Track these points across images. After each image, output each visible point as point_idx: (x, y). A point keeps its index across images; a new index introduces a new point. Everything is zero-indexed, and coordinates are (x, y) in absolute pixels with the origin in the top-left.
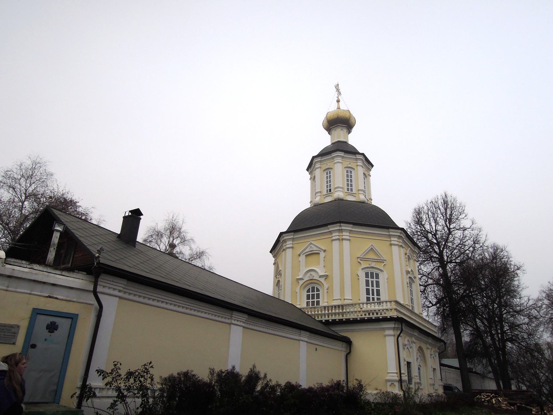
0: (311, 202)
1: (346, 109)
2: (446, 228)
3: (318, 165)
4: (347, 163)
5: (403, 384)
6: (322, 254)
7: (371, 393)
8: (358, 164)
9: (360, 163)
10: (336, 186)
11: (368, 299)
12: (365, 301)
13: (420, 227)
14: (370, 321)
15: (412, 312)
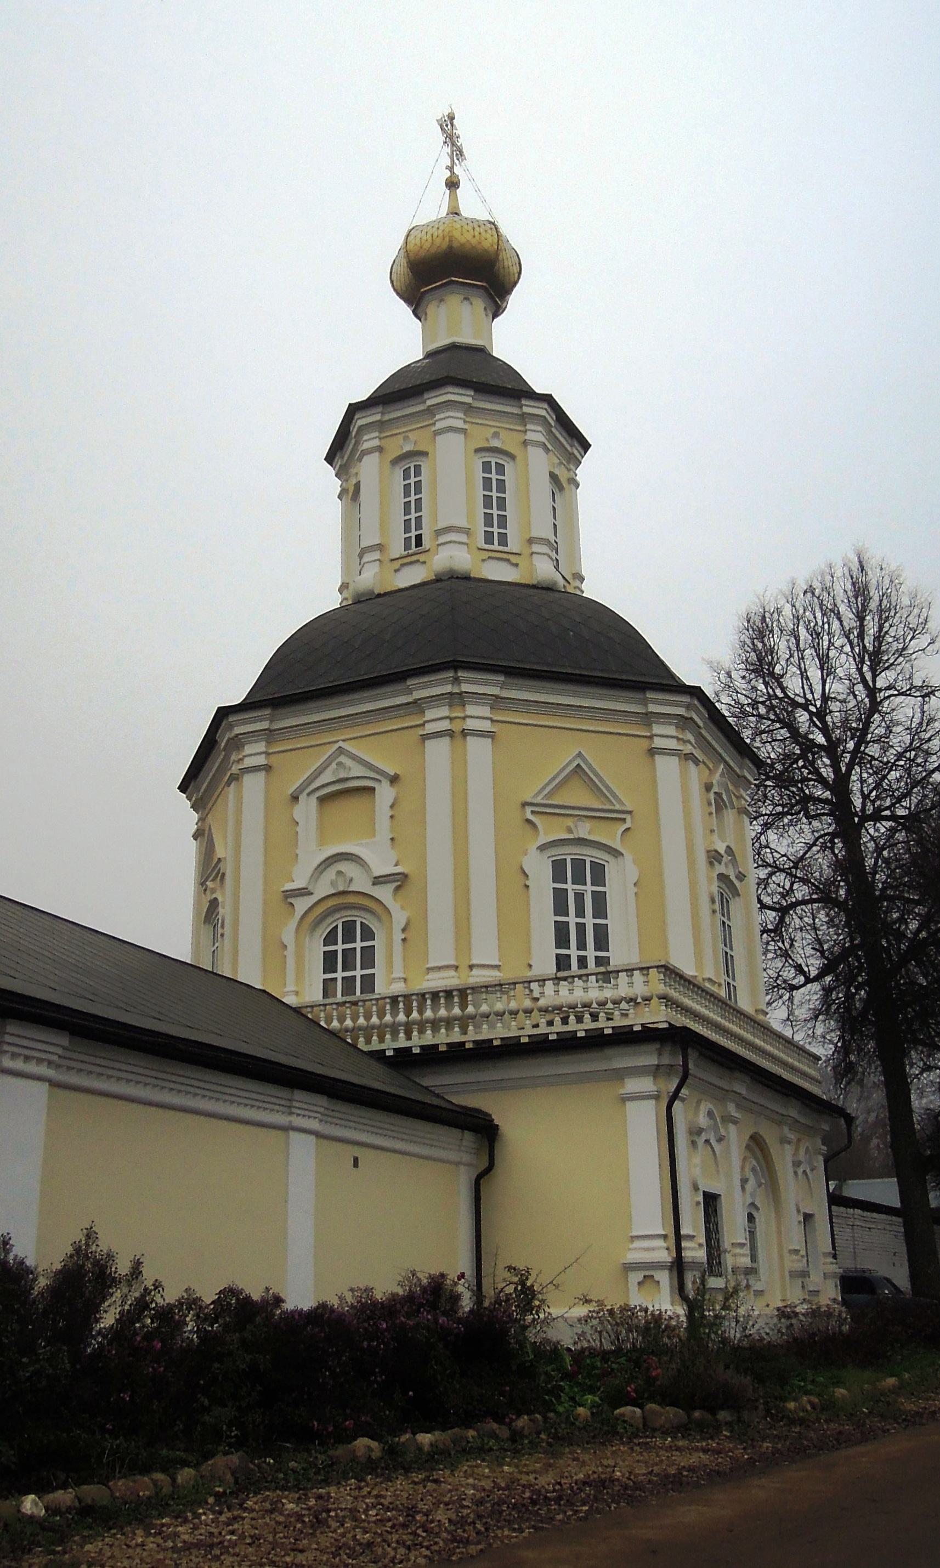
0: (343, 587)
1: (483, 216)
2: (859, 688)
3: (370, 441)
4: (483, 434)
5: (689, 1277)
6: (385, 793)
7: (565, 1317)
8: (530, 436)
9: (536, 433)
10: (441, 525)
11: (562, 962)
12: (551, 969)
13: (766, 684)
14: (568, 1045)
15: (727, 1006)
